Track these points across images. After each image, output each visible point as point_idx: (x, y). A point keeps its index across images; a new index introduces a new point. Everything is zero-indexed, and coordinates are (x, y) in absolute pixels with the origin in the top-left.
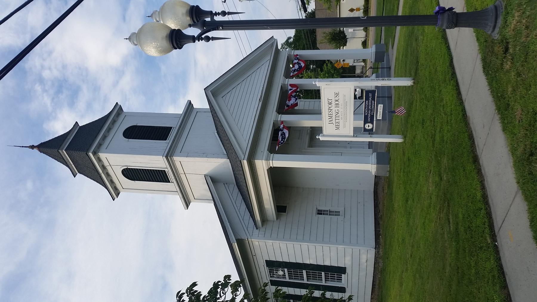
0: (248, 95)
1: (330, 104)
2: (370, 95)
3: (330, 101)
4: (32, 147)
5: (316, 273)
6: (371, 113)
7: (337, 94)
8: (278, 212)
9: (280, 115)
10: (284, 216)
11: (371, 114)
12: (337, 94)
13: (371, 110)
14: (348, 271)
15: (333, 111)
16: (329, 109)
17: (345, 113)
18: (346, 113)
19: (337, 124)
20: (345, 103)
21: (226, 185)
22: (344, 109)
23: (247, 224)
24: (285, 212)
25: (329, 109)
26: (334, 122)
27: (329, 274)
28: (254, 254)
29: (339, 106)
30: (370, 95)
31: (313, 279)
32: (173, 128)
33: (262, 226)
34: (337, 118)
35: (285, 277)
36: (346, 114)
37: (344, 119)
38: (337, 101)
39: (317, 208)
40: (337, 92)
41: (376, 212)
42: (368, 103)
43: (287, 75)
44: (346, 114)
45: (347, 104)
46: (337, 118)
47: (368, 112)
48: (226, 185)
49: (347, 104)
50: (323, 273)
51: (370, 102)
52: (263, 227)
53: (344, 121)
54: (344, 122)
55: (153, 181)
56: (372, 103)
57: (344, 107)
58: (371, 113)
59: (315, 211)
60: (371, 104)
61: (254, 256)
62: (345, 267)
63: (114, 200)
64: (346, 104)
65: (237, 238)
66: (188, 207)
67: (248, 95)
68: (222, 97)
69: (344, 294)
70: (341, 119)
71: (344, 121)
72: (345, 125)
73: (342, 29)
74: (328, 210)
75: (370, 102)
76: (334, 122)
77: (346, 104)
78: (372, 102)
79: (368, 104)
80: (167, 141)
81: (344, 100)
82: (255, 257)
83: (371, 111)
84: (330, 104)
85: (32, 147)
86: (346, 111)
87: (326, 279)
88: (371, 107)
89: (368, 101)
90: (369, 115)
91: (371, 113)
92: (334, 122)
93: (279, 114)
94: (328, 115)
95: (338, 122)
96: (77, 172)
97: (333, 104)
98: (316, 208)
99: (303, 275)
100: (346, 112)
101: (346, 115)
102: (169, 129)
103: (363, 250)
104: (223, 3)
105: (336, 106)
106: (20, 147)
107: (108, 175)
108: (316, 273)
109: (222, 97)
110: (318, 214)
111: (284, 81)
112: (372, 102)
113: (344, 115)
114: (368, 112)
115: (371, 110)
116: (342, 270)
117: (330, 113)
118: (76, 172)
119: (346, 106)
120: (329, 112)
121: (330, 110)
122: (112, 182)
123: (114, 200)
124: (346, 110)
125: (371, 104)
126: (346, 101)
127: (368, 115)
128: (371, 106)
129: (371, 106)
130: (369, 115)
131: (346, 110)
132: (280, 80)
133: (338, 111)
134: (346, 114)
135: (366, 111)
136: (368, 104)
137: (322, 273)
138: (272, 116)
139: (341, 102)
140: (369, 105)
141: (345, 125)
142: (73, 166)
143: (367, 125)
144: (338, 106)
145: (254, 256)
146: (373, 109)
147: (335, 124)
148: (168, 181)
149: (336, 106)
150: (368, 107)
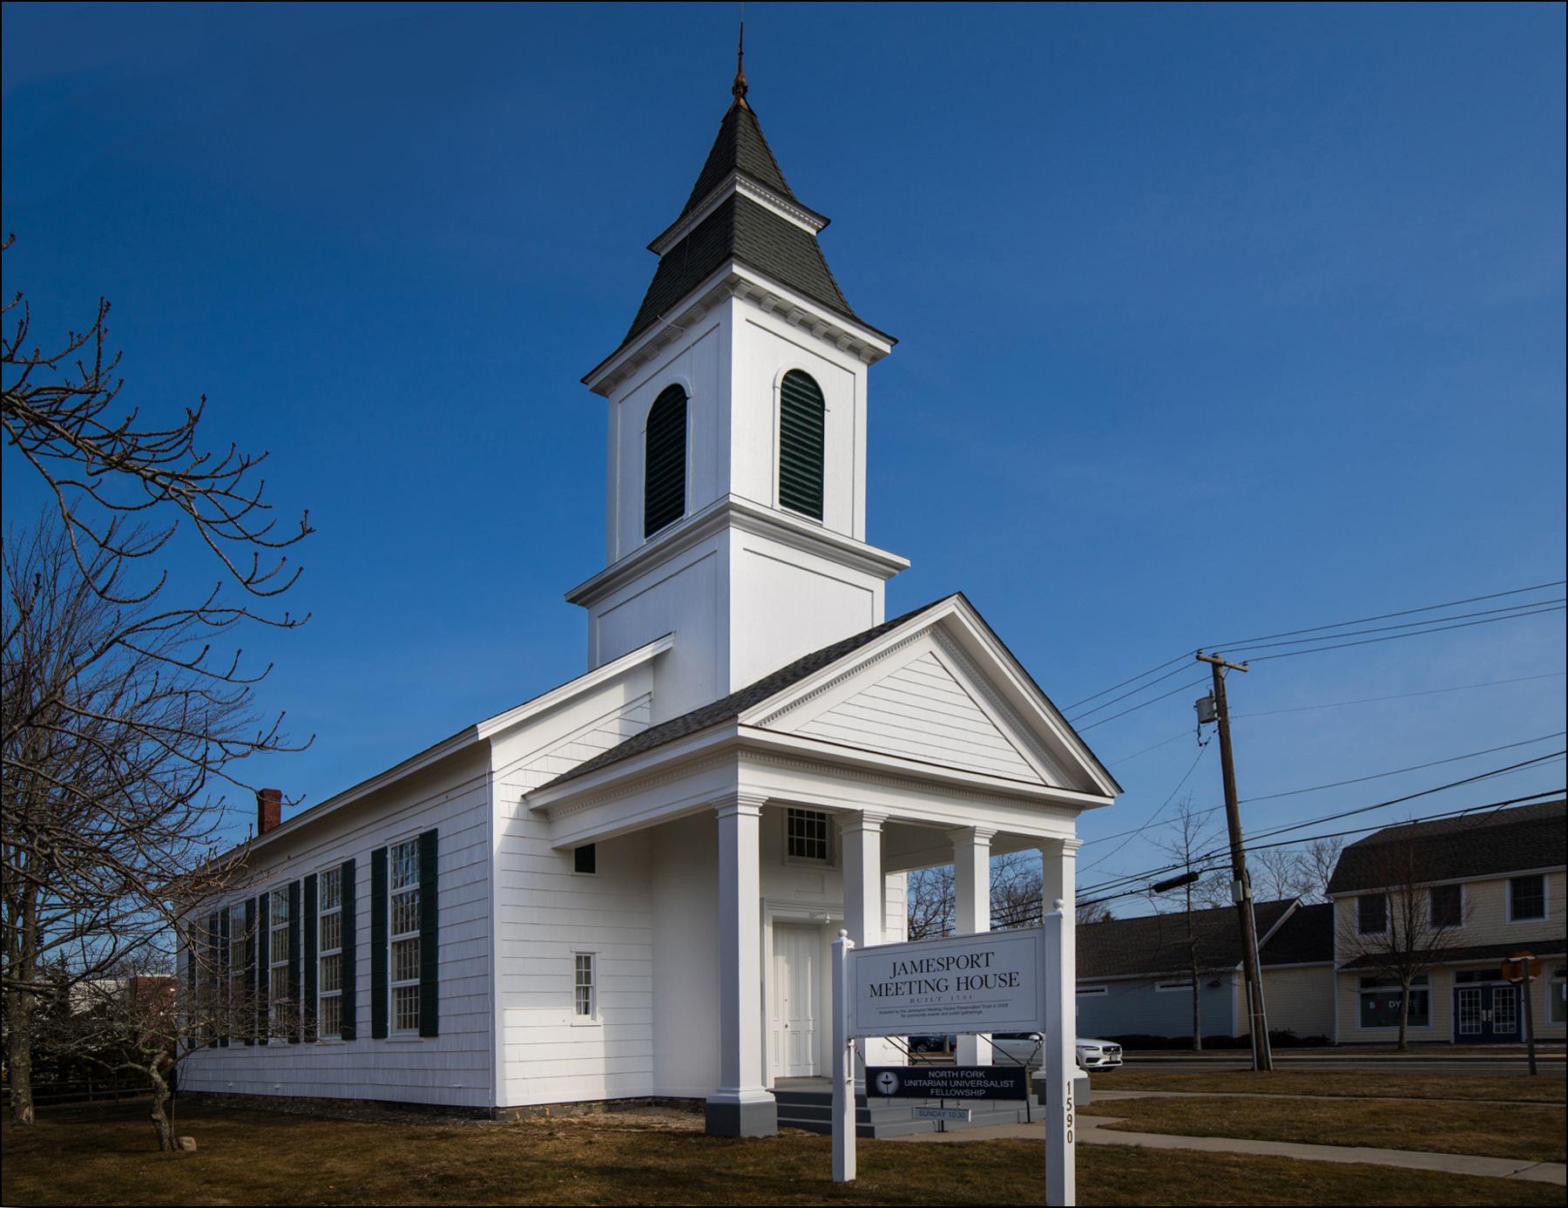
0: (939, 730)
3: (982, 961)
4: (740, 89)
5: (337, 935)
6: (936, 1088)
7: (1009, 980)
9: (877, 827)
11: (931, 1087)
12: (1009, 980)
14: (429, 1044)
15: (945, 974)
16: (951, 960)
20: (974, 1007)
27: (416, 995)
28: (451, 795)
29: (963, 992)
33: (532, 810)
34: (915, 987)
35: (396, 884)
38: (984, 981)
39: (594, 953)
42: (976, 1078)
43: (1003, 843)
45: (971, 1013)
46: (915, 987)
47: (941, 1079)
49: (971, 1013)
50: (416, 982)
51: (979, 1083)
53: (907, 1009)
55: (648, 500)
57: (961, 1005)
59: (584, 948)
60: (970, 1088)
61: (447, 797)
63: (582, 381)
64: (970, 1010)
66: (573, 600)
68: (931, 652)
70: (912, 1001)
72: (891, 1012)
75: (979, 1083)
77: (970, 1010)
78: (980, 1088)
79: (972, 1079)
80: (778, 507)
83: (944, 1088)
85: (740, 89)
88: (958, 1088)
89: (982, 1079)
90: (930, 1083)
91: (936, 1088)
92: (902, 977)
93: (882, 826)
97: (970, 972)
99: (407, 931)
103: (615, 726)
104: (1196, 654)
105: (963, 980)
106: (741, 46)
107: (662, 343)
108: (337, 935)
109: (931, 652)
110: (579, 959)
111: (984, 833)
112: (980, 1088)
113: (926, 1007)
114: (941, 1079)
115: (949, 1088)
116: (429, 1027)
117: (936, 965)
118: (662, 249)
119: (964, 1010)
120: (940, 961)
121: (945, 965)
122: (640, 361)
123: (582, 381)
125: (970, 1088)
127: (926, 1078)
130: (930, 1083)
132: (986, 820)
134: (933, 1012)
135: (942, 1074)
136: (972, 1079)
137: (418, 980)
138: (878, 804)
139: (978, 995)
140: (968, 1080)
141: (891, 1012)
143: (892, 1077)
144: (963, 987)
145: (447, 797)
146: (953, 1092)
147: (891, 981)
150: (959, 1079)
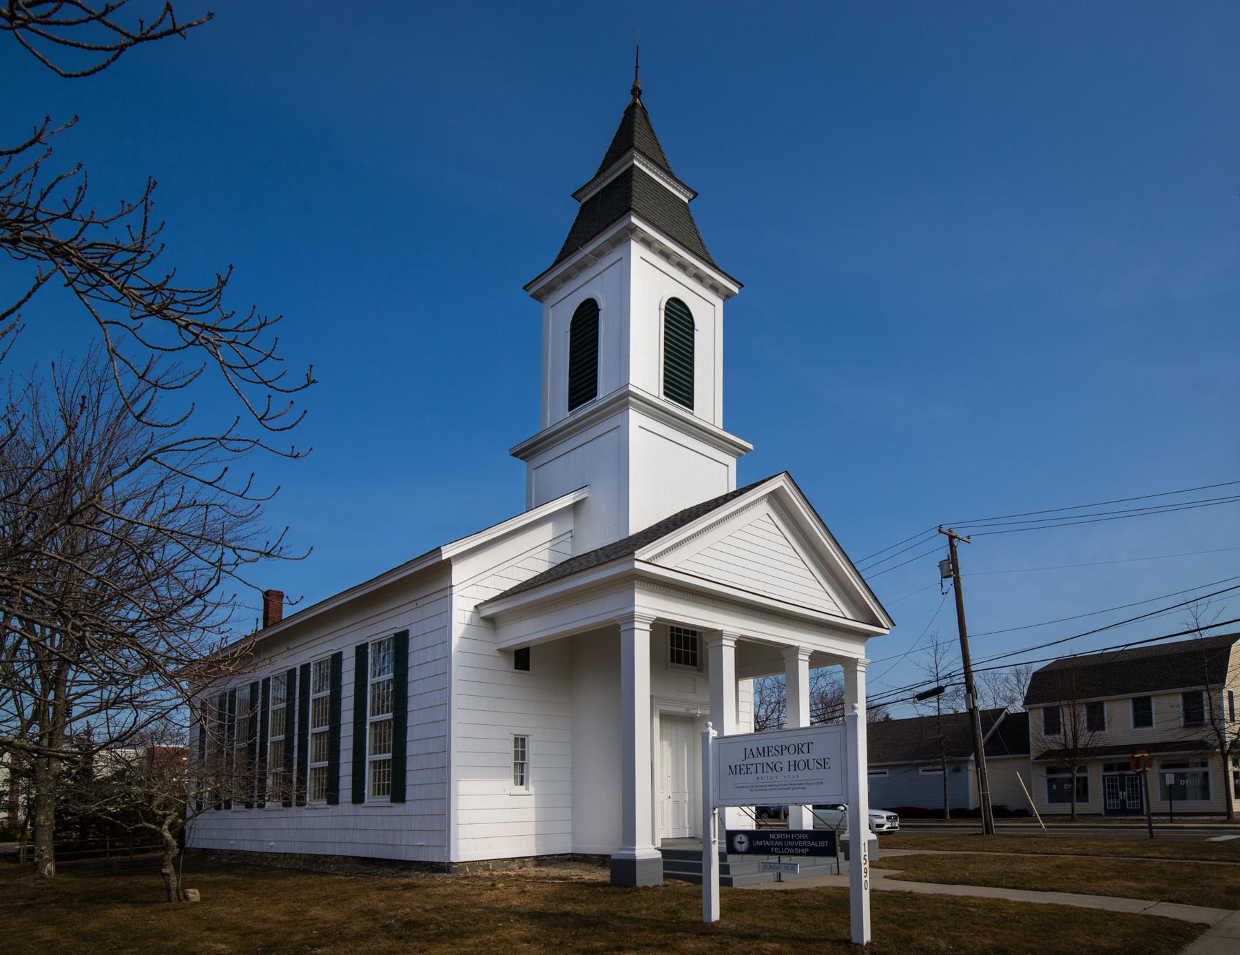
0: (774, 572)
1: (798, 749)
2: (823, 844)
3: (805, 749)
6: (774, 847)
7: (823, 764)
8: (515, 651)
10: (508, 664)
12: (823, 764)
13: (784, 847)
14: (398, 808)
15: (780, 758)
17: (774, 786)
18: (773, 787)
19: (745, 769)
20: (800, 784)
21: (569, 535)
22: (784, 783)
23: (484, 583)
24: (515, 668)
25: (784, 747)
26: (750, 760)
28: (420, 603)
29: (792, 773)
30: (823, 844)
31: (375, 773)
32: (692, 411)
34: (760, 768)
36: (772, 789)
37: (757, 784)
38: (807, 764)
39: (527, 736)
40: (831, 763)
41: (527, 860)
42: (802, 840)
43: (818, 659)
44: (772, 789)
45: (798, 788)
46: (760, 768)
47: (778, 840)
48: (569, 535)
49: (798, 788)
51: (805, 843)
52: (481, 621)
54: (749, 785)
56: (801, 848)
58: (777, 846)
59: (521, 731)
60: (798, 847)
62: (407, 802)
63: (524, 288)
64: (797, 786)
65: (452, 561)
66: (515, 455)
67: (774, 572)
69: (350, 800)
70: (758, 779)
71: (752, 785)
72: (743, 787)
73: (3, 802)
74: (524, 760)
75: (805, 843)
76: (748, 761)
77: (797, 786)
78: (804, 847)
79: (799, 840)
81: (809, 782)
82: (413, 605)
84: (798, 749)
86: (780, 787)
87: (376, 764)
88: (790, 847)
89: (806, 840)
90: (771, 843)
91: (774, 847)
92: (750, 760)
94: (766, 746)
95: (749, 772)
96: (583, 201)
98: (527, 734)
100: (776, 787)
101: (768, 788)
102: (688, 401)
104: (938, 528)
105: (792, 763)
106: (637, 61)
107: (582, 267)
110: (516, 740)
112: (804, 847)
113: (768, 784)
114: (778, 840)
116: (398, 793)
117: (774, 751)
121: (780, 751)
123: (524, 288)
124: (782, 789)
125: (798, 847)
126: (807, 786)
127: (768, 839)
128: (795, 847)
129: (795, 847)
130: (771, 843)
131: (782, 789)
133: (778, 769)
135: (779, 836)
137: (391, 754)
138: (732, 626)
140: (797, 841)
142: (599, 189)
143: (744, 838)
144: (792, 768)
146: (787, 851)
147: (745, 763)
148: (571, 407)
149: (792, 763)
150: (791, 840)
